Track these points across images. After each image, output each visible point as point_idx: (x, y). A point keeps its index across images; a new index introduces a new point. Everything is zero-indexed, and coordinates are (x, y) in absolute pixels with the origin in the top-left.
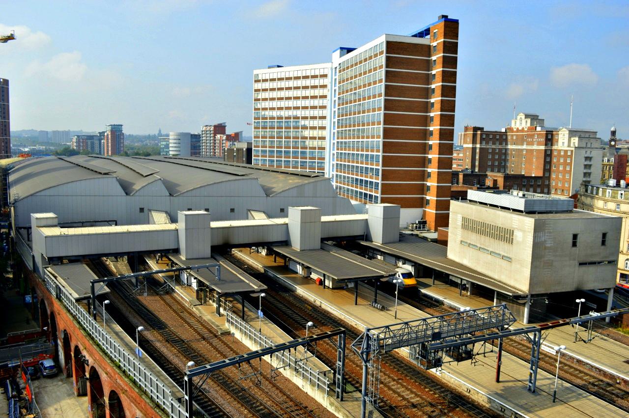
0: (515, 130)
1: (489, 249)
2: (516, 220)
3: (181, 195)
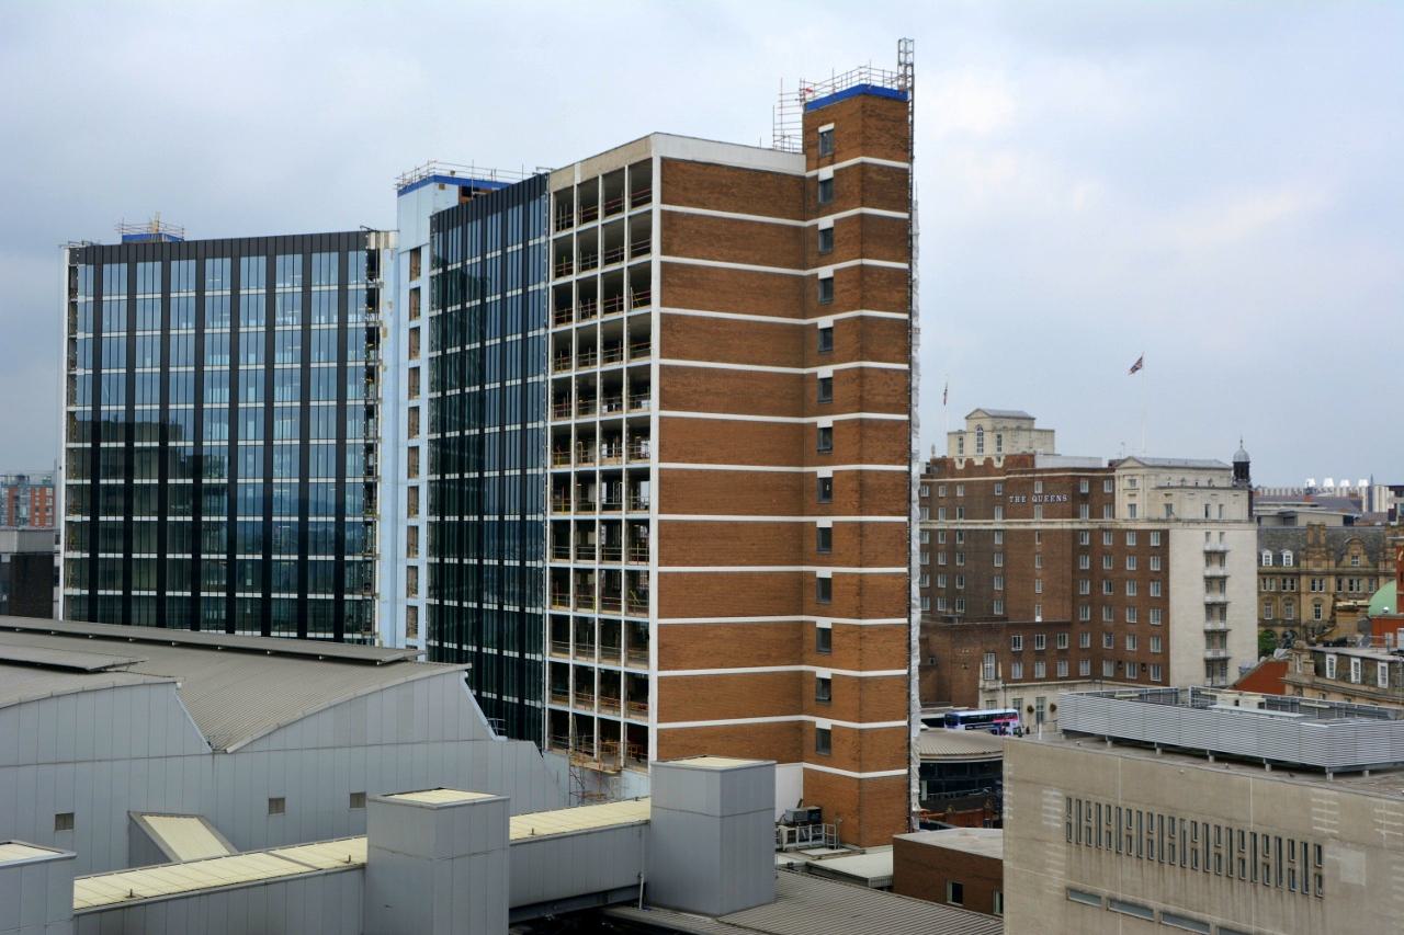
0: (960, 467)
1: (1206, 917)
2: (1330, 807)
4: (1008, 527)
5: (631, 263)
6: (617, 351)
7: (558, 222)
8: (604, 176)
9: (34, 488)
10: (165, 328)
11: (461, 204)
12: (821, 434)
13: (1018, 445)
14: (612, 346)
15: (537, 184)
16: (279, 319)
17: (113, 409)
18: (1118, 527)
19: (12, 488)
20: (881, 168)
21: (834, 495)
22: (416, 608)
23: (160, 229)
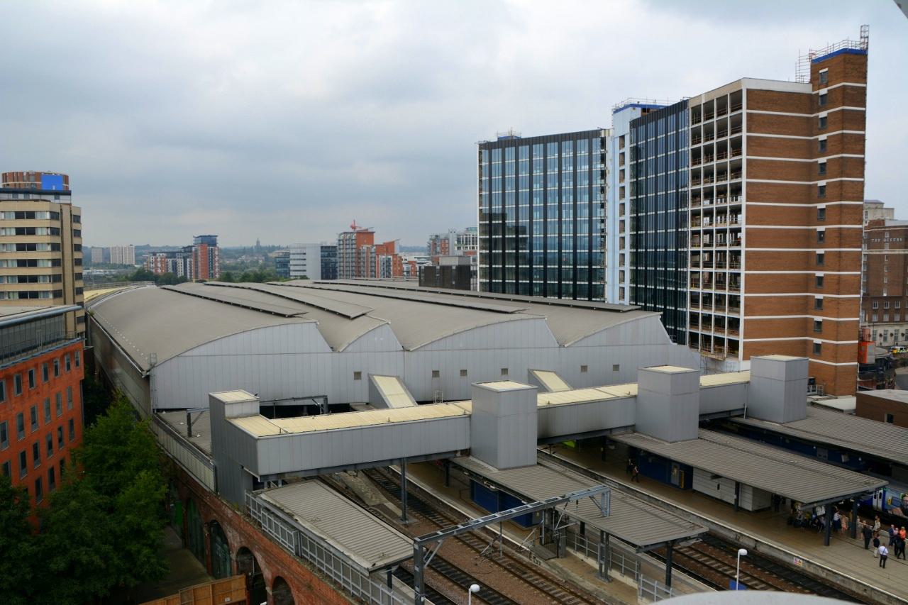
4: (870, 253)
8: (717, 99)
10: (517, 173)
15: (682, 105)
16: (564, 168)
17: (497, 208)
19: (434, 240)
22: (624, 288)
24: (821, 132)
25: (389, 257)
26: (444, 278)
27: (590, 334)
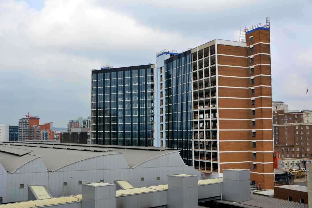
3: (59, 170)
4: (279, 125)
5: (199, 70)
6: (208, 85)
7: (193, 59)
8: (204, 49)
9: (75, 123)
11: (170, 58)
12: (252, 101)
13: (281, 108)
14: (207, 84)
15: (188, 52)
18: (304, 125)
19: (71, 123)
20: (264, 44)
21: (255, 114)
22: (163, 141)
23: (109, 66)
24: (251, 64)
25: (47, 131)
26: (73, 138)
27: (146, 161)
